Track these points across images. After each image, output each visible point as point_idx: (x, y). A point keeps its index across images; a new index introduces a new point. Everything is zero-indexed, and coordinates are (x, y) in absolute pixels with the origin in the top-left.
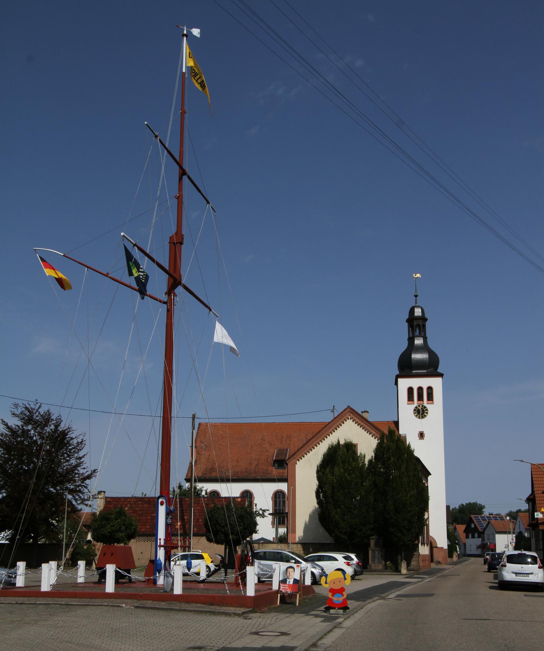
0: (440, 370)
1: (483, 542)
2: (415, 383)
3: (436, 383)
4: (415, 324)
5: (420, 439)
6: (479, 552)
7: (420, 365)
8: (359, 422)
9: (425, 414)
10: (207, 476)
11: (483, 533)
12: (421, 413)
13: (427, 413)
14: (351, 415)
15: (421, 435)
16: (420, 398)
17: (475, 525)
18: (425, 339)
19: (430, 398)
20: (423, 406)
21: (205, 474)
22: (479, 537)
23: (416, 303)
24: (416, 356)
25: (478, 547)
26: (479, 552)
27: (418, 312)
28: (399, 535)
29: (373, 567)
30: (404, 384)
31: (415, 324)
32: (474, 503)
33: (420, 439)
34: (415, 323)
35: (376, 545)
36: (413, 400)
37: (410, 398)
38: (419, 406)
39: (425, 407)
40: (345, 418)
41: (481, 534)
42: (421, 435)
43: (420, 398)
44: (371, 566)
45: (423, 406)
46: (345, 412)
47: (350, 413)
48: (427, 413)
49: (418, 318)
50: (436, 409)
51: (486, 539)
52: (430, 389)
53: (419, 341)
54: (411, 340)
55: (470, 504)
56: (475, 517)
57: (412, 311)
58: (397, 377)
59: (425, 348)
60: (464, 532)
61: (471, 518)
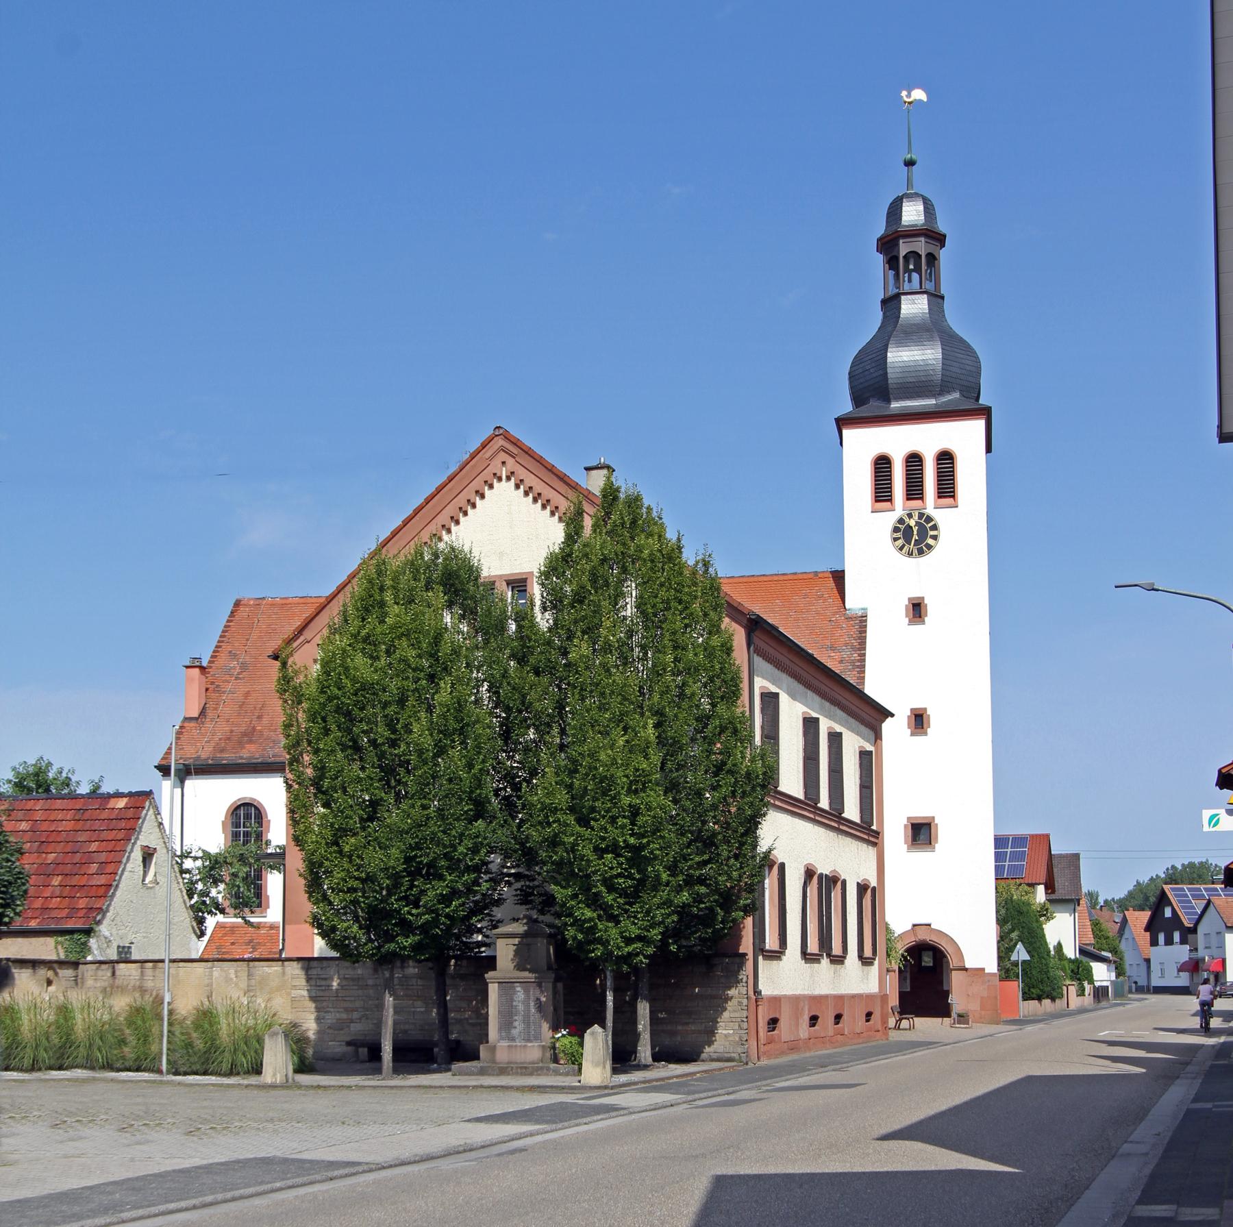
0: (983, 401)
1: (1194, 955)
2: (897, 441)
3: (964, 438)
4: (903, 253)
5: (911, 622)
6: (1183, 980)
7: (917, 385)
8: (539, 487)
9: (930, 541)
10: (228, 757)
11: (1194, 930)
12: (915, 537)
13: (935, 538)
14: (510, 461)
15: (917, 610)
16: (914, 489)
17: (1174, 911)
18: (936, 298)
19: (947, 488)
20: (921, 515)
21: (222, 751)
22: (1183, 941)
23: (909, 184)
24: (900, 356)
25: (1181, 969)
26: (1183, 980)
27: (912, 214)
28: (589, 914)
29: (502, 1056)
30: (862, 445)
31: (903, 253)
32: (1201, 863)
33: (911, 622)
34: (904, 248)
35: (523, 959)
36: (889, 499)
37: (882, 493)
38: (910, 516)
39: (929, 519)
40: (487, 475)
41: (1188, 934)
42: (917, 610)
43: (914, 489)
44: (493, 1049)
45: (921, 515)
46: (487, 453)
47: (503, 456)
48: (935, 538)
49: (913, 233)
50: (964, 525)
51: (1201, 946)
52: (946, 459)
53: (914, 307)
54: (891, 303)
55: (1191, 865)
56: (1173, 889)
57: (895, 211)
58: (842, 423)
59: (933, 326)
60: (1147, 930)
61: (1163, 893)
